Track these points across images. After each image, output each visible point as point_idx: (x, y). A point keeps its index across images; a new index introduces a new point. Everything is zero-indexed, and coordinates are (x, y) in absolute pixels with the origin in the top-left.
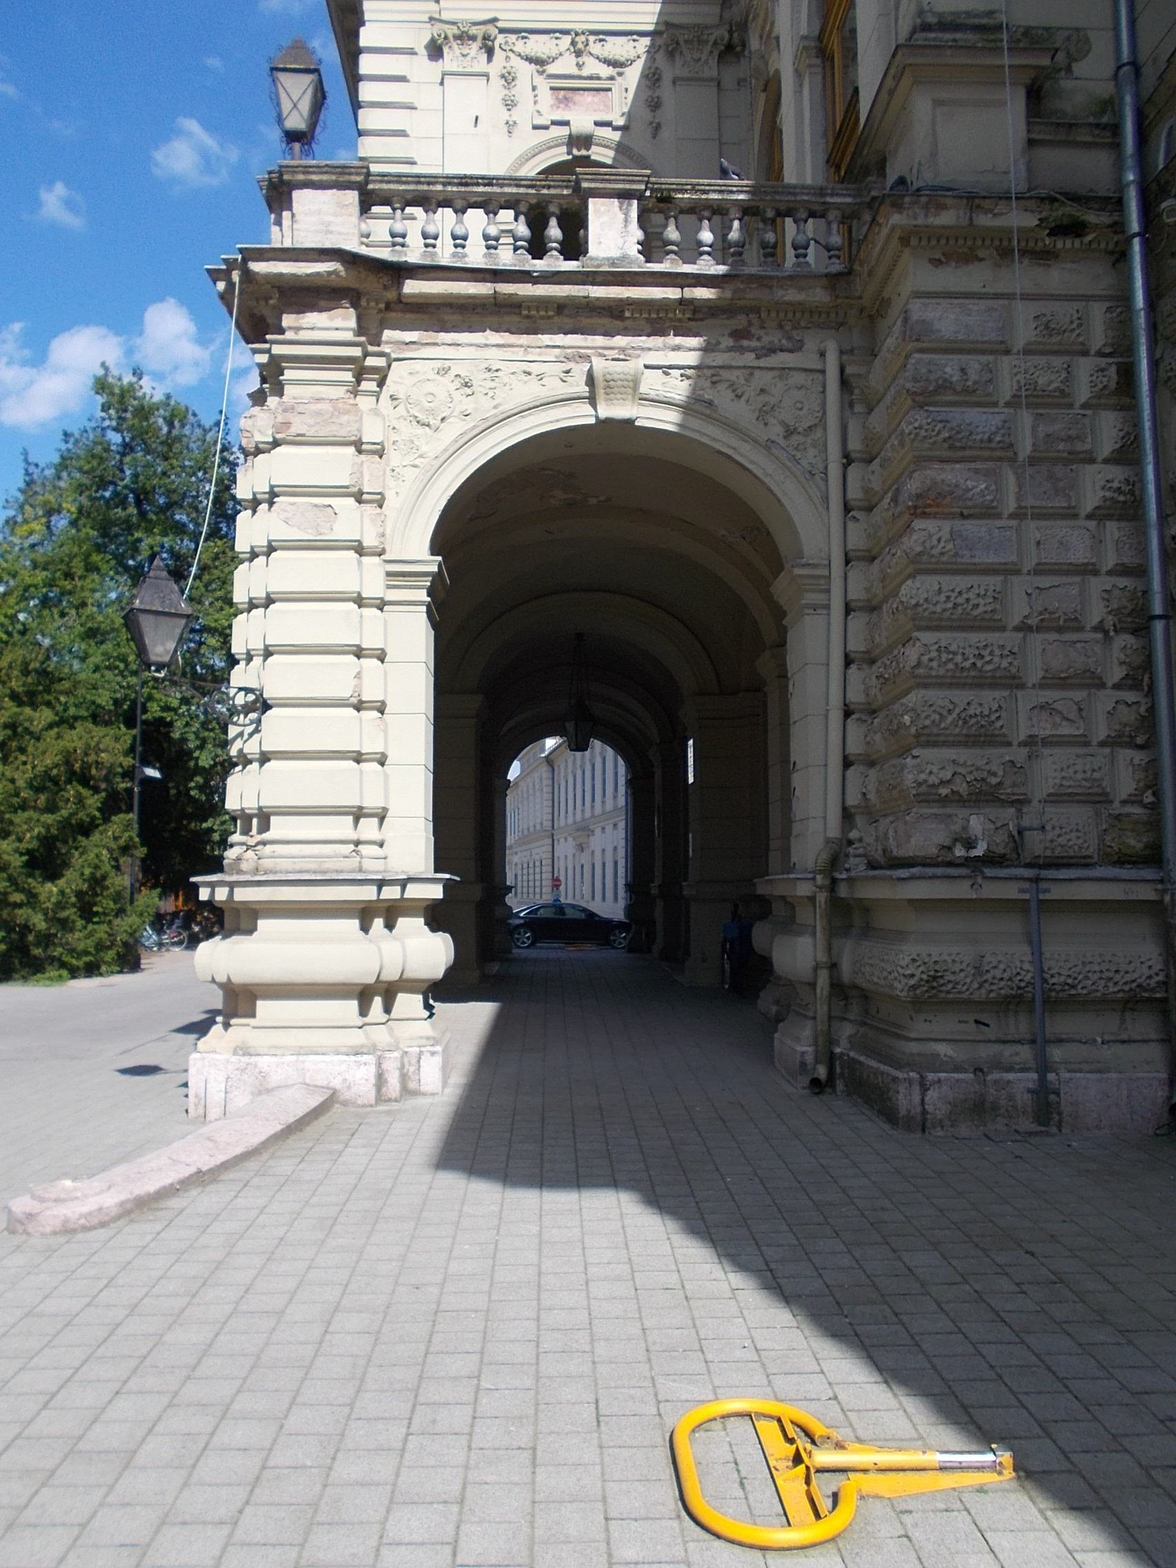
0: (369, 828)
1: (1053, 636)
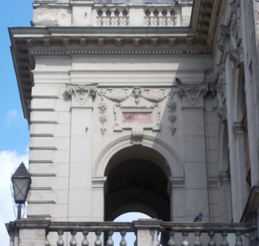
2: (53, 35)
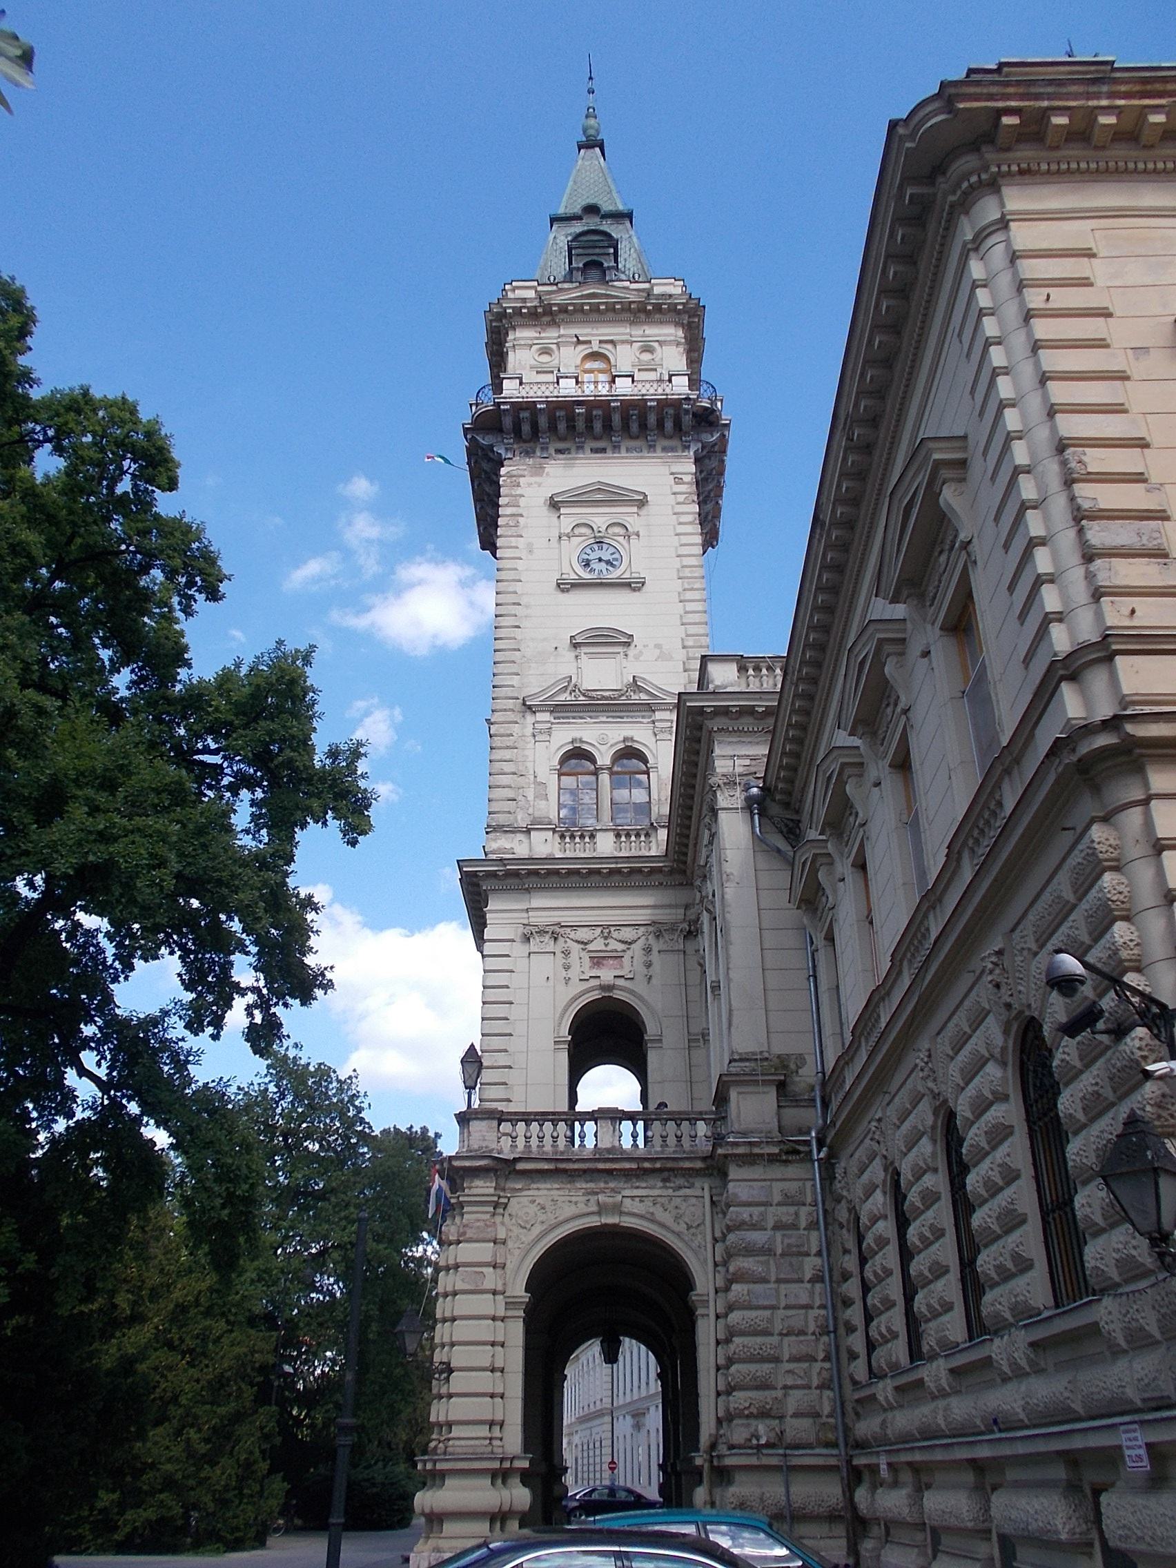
0: (496, 1432)
1: (793, 1338)
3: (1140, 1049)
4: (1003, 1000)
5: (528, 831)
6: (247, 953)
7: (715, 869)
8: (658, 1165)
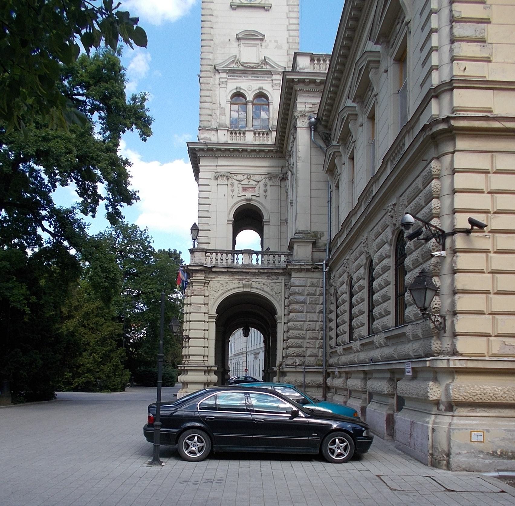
0: (206, 358)
1: (311, 331)
2: (209, 147)
3: (432, 246)
4: (393, 223)
5: (217, 130)
6: (103, 183)
7: (294, 153)
8: (266, 271)
